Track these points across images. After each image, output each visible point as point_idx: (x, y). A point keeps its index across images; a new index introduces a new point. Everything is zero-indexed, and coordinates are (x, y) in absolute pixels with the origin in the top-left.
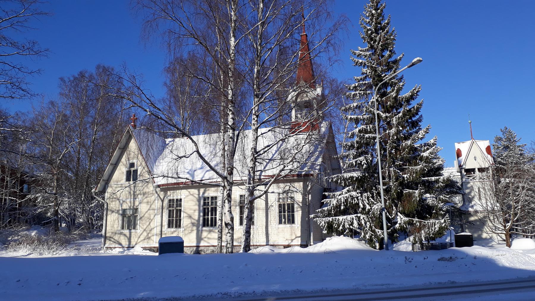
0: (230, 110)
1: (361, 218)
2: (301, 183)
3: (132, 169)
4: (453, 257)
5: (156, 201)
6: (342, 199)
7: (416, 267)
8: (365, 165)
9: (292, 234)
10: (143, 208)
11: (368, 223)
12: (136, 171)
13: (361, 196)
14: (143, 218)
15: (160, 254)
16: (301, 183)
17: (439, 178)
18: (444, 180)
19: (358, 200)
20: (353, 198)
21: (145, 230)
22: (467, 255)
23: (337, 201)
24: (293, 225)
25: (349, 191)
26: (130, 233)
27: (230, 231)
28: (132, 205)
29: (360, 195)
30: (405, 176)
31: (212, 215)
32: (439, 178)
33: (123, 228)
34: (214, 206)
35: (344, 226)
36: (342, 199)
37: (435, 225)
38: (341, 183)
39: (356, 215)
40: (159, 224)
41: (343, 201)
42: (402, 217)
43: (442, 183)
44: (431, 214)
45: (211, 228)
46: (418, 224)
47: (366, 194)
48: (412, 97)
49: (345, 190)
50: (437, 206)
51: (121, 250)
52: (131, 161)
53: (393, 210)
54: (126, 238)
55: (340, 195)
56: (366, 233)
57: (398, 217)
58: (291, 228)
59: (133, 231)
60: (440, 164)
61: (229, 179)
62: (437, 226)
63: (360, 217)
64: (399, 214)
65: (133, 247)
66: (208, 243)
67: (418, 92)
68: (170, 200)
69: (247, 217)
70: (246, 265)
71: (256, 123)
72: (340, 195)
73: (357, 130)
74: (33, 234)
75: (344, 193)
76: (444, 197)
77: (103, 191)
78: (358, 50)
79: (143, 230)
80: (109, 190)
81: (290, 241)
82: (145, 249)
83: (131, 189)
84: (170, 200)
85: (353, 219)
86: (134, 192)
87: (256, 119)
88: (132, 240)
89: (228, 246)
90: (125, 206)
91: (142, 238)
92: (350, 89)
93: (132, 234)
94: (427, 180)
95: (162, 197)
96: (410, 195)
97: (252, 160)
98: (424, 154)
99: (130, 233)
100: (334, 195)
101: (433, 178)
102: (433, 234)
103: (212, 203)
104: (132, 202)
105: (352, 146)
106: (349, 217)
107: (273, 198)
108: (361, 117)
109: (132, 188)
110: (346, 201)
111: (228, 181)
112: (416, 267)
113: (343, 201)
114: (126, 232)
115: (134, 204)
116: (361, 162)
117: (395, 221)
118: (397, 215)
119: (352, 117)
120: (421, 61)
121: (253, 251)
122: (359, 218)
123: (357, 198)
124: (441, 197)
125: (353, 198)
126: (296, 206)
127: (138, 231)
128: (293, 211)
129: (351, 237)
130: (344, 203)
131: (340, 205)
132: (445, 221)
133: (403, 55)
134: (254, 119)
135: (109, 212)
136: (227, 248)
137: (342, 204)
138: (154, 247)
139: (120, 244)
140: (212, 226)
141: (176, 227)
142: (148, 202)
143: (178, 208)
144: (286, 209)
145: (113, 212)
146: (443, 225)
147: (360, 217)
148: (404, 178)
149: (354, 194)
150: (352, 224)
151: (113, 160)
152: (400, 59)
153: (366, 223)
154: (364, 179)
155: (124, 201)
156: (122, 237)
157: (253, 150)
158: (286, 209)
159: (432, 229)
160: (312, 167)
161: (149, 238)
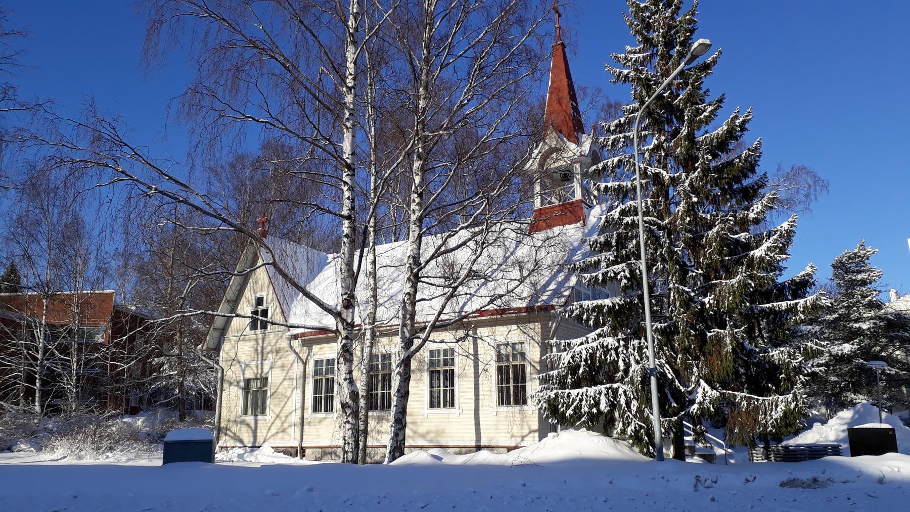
0: (345, 183)
1: (621, 391)
2: (538, 326)
3: (260, 308)
4: (822, 478)
5: (295, 365)
6: (584, 352)
7: (713, 500)
8: (624, 281)
9: (522, 425)
10: (275, 378)
11: (634, 402)
12: (265, 313)
13: (626, 347)
14: (276, 395)
15: (166, 460)
16: (538, 326)
17: (797, 304)
18: (805, 307)
19: (617, 354)
20: (606, 350)
21: (278, 416)
22: (860, 475)
23: (573, 357)
24: (525, 407)
25: (599, 336)
26: (256, 421)
27: (350, 419)
28: (260, 371)
29: (622, 343)
30: (706, 300)
31: (383, 389)
32: (797, 304)
33: (245, 412)
34: (386, 372)
35: (579, 407)
36: (584, 352)
37: (777, 406)
38: (588, 319)
39: (608, 386)
40: (299, 405)
41: (584, 356)
42: (708, 388)
43: (803, 313)
44: (777, 383)
45: (382, 413)
46: (744, 403)
47: (636, 342)
48: (731, 134)
49: (593, 335)
50: (789, 364)
51: (241, 451)
52: (259, 295)
53: (692, 373)
54: (250, 431)
55: (582, 344)
56: (626, 424)
57: (700, 390)
58: (522, 413)
59: (260, 417)
60: (808, 275)
61: (344, 316)
62: (782, 407)
63: (618, 389)
64: (702, 382)
65: (259, 447)
66: (378, 440)
67: (744, 122)
68: (316, 362)
69: (398, 391)
70: (311, 490)
71: (417, 208)
72: (582, 344)
73: (618, 210)
74: (139, 423)
75: (590, 340)
76: (817, 344)
77: (217, 349)
78: (624, 51)
79: (274, 416)
80: (226, 346)
81: (519, 440)
82: (277, 449)
83: (258, 344)
84: (316, 362)
85: (600, 393)
86: (263, 348)
87: (417, 200)
88: (259, 434)
89: (347, 448)
90: (249, 374)
91: (273, 431)
92: (609, 130)
93: (259, 422)
94: (770, 309)
95: (304, 356)
96: (719, 340)
97: (409, 279)
98: (756, 251)
99: (256, 421)
100: (569, 344)
101: (784, 305)
102: (773, 427)
103: (383, 364)
104: (260, 366)
105: (607, 246)
106: (592, 390)
107: (487, 355)
108: (629, 185)
109: (260, 342)
110: (592, 356)
111: (343, 320)
112: (713, 500)
113: (584, 356)
114: (250, 419)
115: (262, 369)
116: (616, 274)
117: (691, 397)
118: (698, 384)
119: (609, 185)
120: (710, 45)
121: (410, 457)
122: (615, 392)
123: (616, 349)
124: (809, 344)
125: (608, 350)
126: (528, 369)
127: (268, 418)
128: (524, 380)
129: (589, 429)
130: (586, 360)
131: (579, 366)
132: (795, 396)
133: (720, 53)
134: (414, 201)
135: (225, 385)
136: (346, 452)
137: (583, 363)
138: (291, 447)
139: (241, 441)
140: (383, 409)
141: (326, 411)
142: (283, 366)
143: (330, 376)
144: (511, 376)
145: (231, 384)
146: (792, 406)
147: (618, 389)
148: (703, 304)
149: (610, 341)
150: (597, 404)
151: (230, 294)
152: (715, 61)
153: (628, 404)
154: (630, 310)
155: (247, 365)
156: (244, 429)
157: (411, 261)
158: (511, 376)
159: (770, 415)
160: (557, 293)
161: (284, 431)
